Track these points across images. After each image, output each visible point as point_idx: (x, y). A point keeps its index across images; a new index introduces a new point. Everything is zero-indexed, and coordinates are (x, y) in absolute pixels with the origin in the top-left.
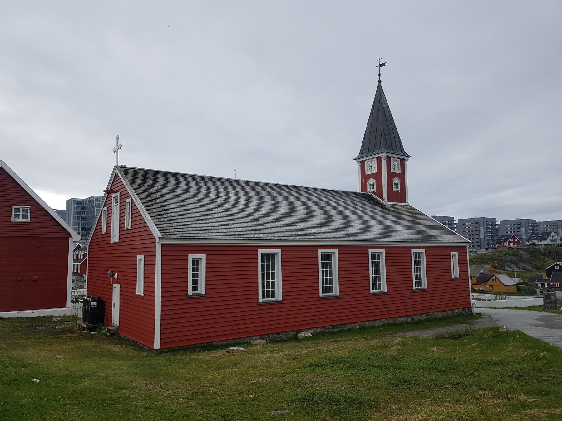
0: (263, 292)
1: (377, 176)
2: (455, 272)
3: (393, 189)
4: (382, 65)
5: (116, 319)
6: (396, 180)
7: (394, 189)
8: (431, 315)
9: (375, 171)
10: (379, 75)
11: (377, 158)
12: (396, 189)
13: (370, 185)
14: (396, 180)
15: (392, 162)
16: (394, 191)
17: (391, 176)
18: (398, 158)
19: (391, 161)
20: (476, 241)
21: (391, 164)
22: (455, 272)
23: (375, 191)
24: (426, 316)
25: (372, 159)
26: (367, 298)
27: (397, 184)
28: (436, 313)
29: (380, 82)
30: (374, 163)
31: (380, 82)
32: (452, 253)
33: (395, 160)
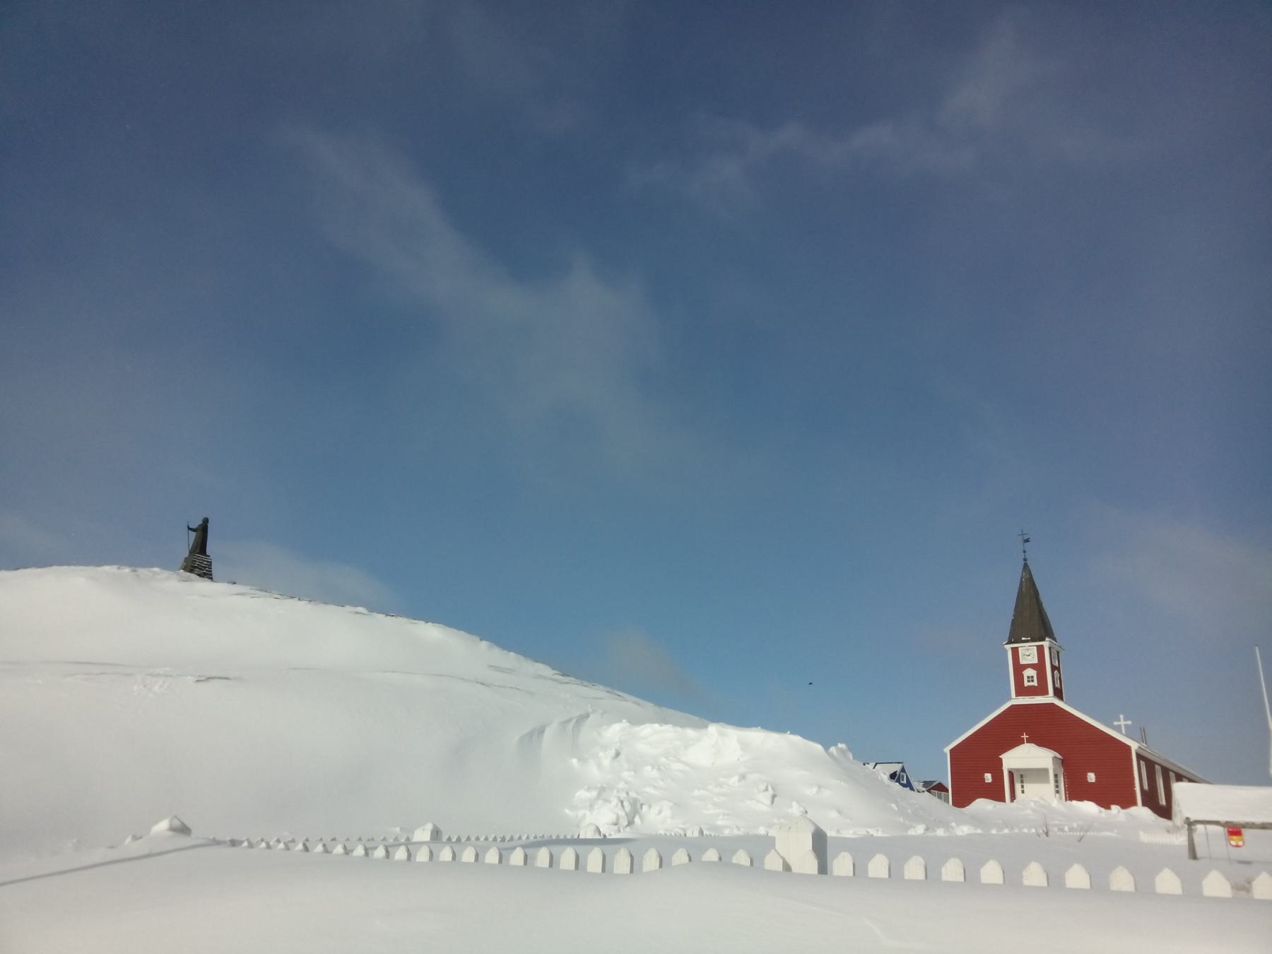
4: (1027, 541)
7: (1026, 684)
11: (1037, 646)
13: (1028, 677)
29: (1025, 560)
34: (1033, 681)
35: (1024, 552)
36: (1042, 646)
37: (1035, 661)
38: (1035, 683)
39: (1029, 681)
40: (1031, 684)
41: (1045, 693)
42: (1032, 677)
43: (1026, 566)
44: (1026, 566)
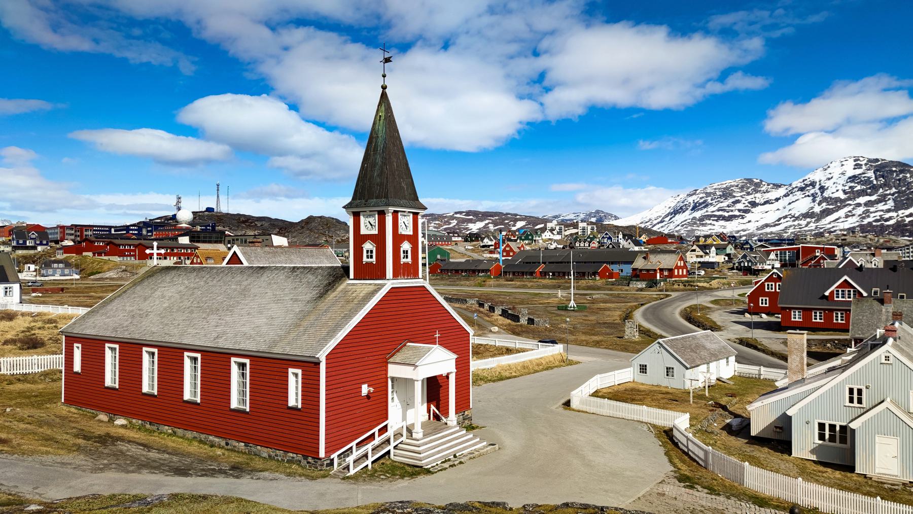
0: (62, 373)
1: (379, 239)
2: (294, 398)
3: (364, 260)
5: (409, 344)
6: (406, 246)
7: (365, 259)
8: (250, 447)
9: (410, 232)
10: (384, 76)
12: (370, 260)
14: (406, 246)
15: (401, 219)
16: (402, 263)
17: (398, 239)
18: (409, 212)
19: (400, 217)
20: (648, 366)
21: (399, 221)
22: (294, 398)
23: (374, 263)
24: (245, 446)
25: (371, 211)
26: (179, 404)
27: (407, 251)
28: (259, 447)
29: (384, 88)
30: (375, 220)
31: (384, 88)
32: (291, 370)
33: (405, 216)
34: (371, 257)
35: (384, 76)
36: (384, 211)
37: (375, 231)
38: (374, 260)
39: (368, 257)
40: (370, 260)
41: (415, 275)
42: (372, 252)
43: (384, 96)
44: (384, 96)
